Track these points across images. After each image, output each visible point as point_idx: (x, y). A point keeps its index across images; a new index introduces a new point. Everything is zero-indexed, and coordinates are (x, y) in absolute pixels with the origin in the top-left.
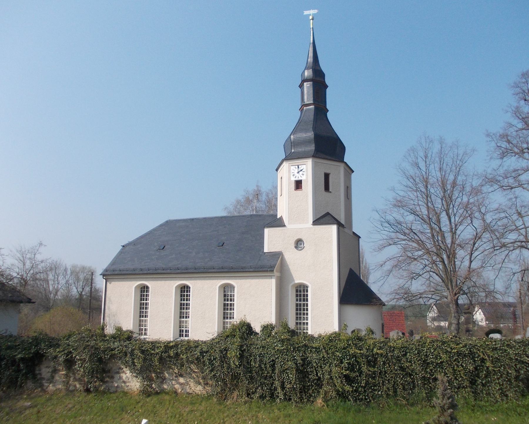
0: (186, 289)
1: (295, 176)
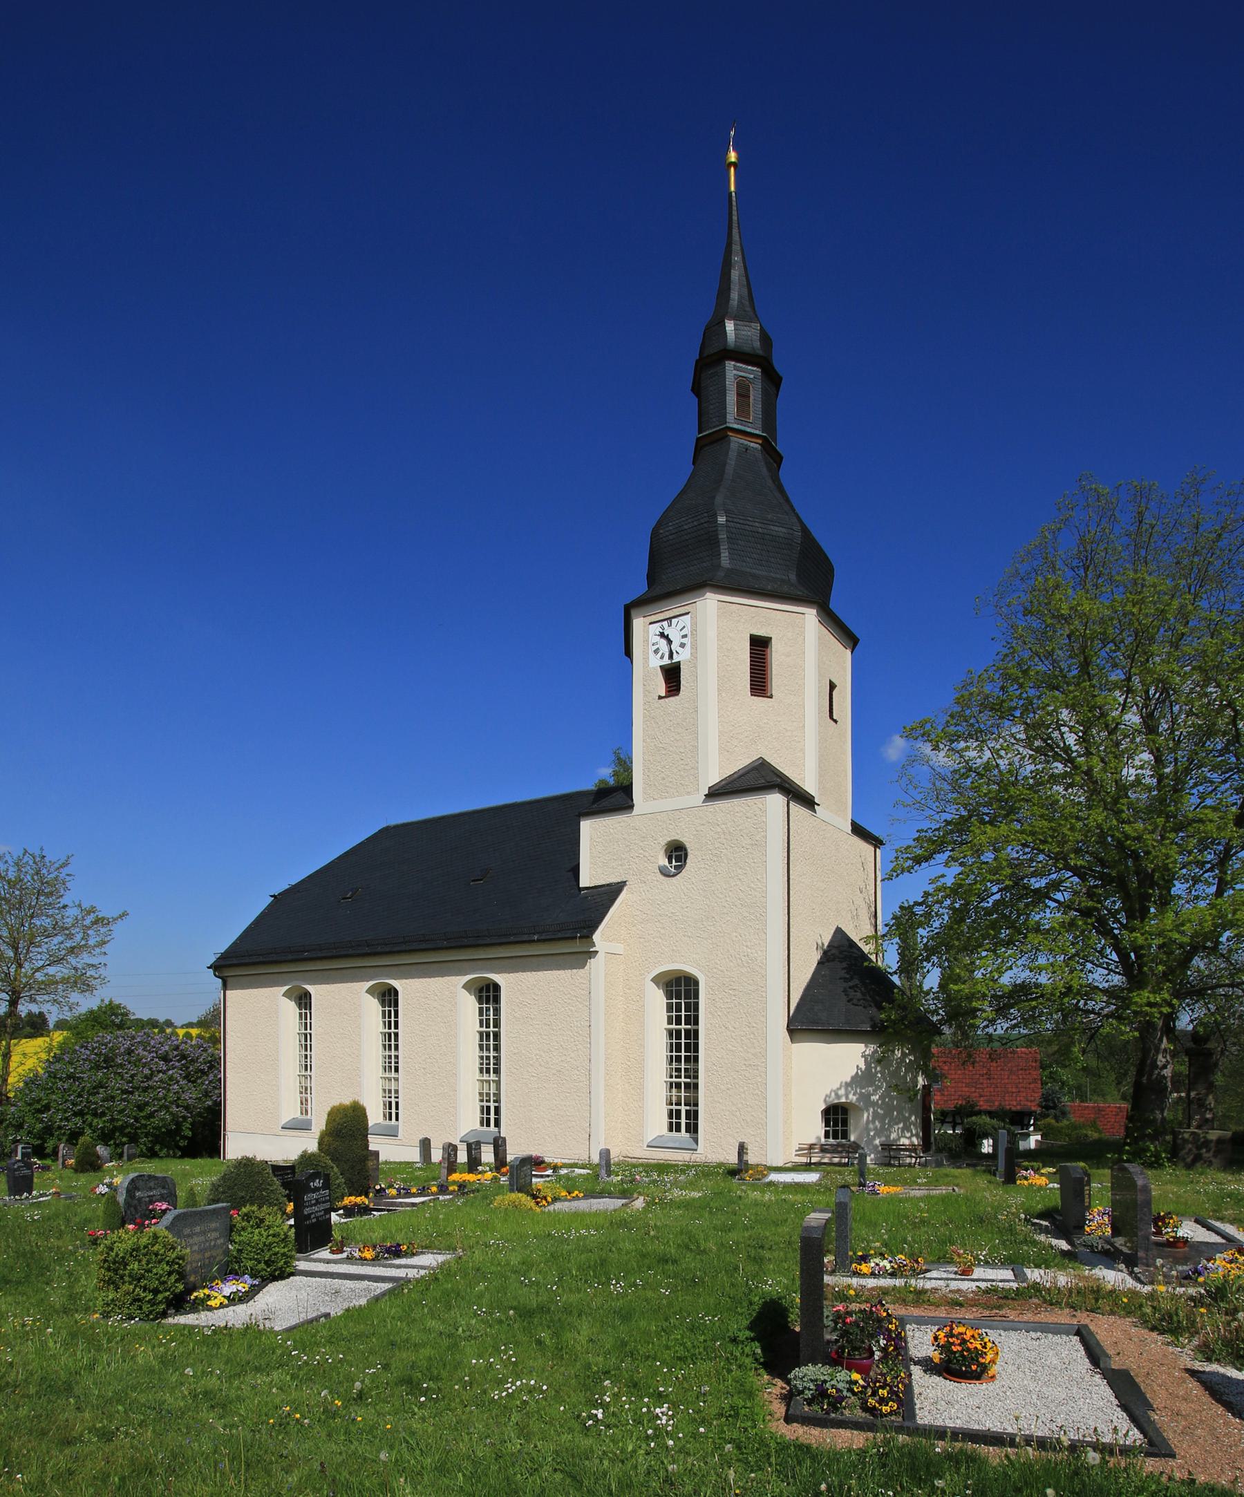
0: (491, 994)
1: (660, 654)
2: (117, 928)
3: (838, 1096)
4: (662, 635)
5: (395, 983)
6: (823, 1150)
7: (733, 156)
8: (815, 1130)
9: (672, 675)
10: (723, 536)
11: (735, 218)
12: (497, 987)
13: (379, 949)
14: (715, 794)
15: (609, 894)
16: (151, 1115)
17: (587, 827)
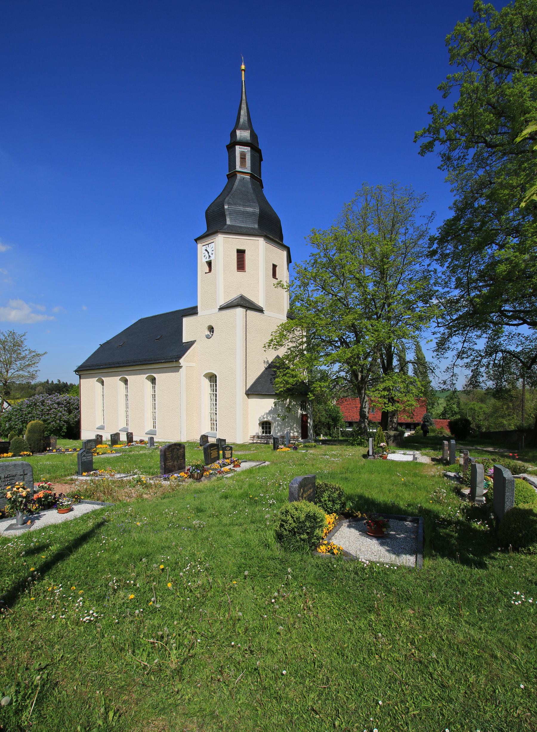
2: (42, 358)
3: (264, 418)
4: (206, 250)
5: (155, 375)
6: (258, 437)
7: (243, 67)
8: (258, 430)
9: (209, 264)
10: (227, 213)
11: (244, 90)
12: (155, 379)
13: (121, 365)
14: (222, 309)
15: (191, 344)
16: (50, 423)
17: (185, 320)
